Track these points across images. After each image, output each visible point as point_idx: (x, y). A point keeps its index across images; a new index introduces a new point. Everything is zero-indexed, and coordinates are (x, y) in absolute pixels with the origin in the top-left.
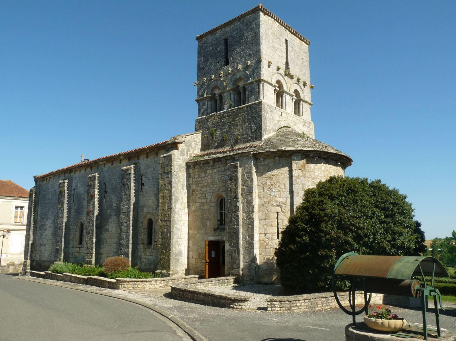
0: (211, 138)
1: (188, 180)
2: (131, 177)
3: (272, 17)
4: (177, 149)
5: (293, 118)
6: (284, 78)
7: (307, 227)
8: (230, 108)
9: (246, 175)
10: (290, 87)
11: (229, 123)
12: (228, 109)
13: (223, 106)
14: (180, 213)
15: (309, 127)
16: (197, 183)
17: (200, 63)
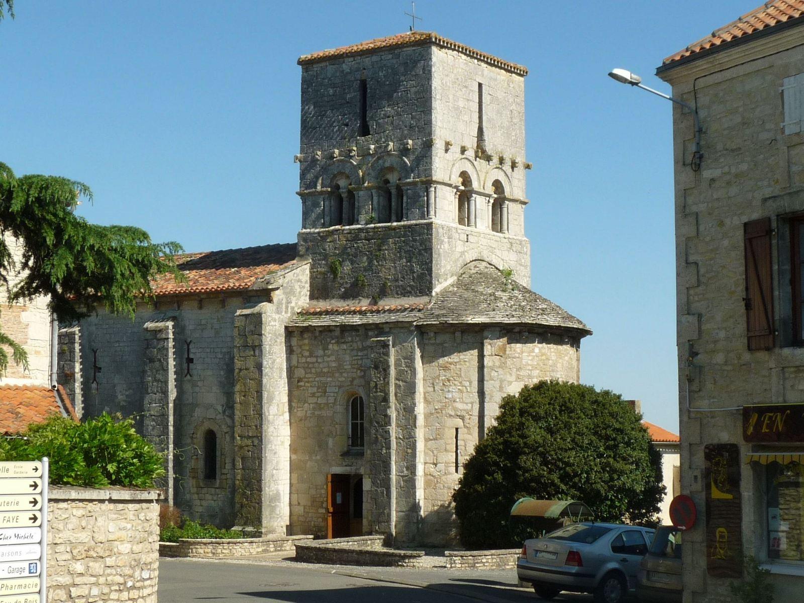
0: (332, 276)
1: (289, 360)
2: (168, 346)
3: (454, 50)
4: (270, 300)
5: (489, 241)
6: (474, 165)
7: (500, 461)
8: (371, 222)
9: (403, 361)
10: (485, 179)
11: (368, 252)
12: (367, 224)
13: (356, 216)
14: (276, 423)
15: (520, 252)
16: (306, 365)
17: (307, 117)
